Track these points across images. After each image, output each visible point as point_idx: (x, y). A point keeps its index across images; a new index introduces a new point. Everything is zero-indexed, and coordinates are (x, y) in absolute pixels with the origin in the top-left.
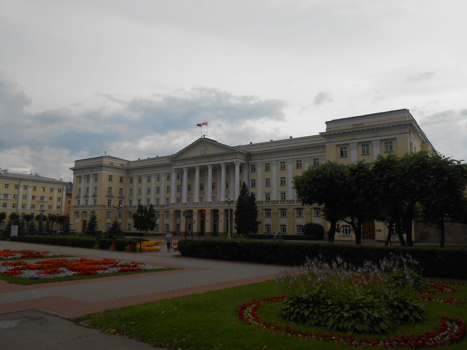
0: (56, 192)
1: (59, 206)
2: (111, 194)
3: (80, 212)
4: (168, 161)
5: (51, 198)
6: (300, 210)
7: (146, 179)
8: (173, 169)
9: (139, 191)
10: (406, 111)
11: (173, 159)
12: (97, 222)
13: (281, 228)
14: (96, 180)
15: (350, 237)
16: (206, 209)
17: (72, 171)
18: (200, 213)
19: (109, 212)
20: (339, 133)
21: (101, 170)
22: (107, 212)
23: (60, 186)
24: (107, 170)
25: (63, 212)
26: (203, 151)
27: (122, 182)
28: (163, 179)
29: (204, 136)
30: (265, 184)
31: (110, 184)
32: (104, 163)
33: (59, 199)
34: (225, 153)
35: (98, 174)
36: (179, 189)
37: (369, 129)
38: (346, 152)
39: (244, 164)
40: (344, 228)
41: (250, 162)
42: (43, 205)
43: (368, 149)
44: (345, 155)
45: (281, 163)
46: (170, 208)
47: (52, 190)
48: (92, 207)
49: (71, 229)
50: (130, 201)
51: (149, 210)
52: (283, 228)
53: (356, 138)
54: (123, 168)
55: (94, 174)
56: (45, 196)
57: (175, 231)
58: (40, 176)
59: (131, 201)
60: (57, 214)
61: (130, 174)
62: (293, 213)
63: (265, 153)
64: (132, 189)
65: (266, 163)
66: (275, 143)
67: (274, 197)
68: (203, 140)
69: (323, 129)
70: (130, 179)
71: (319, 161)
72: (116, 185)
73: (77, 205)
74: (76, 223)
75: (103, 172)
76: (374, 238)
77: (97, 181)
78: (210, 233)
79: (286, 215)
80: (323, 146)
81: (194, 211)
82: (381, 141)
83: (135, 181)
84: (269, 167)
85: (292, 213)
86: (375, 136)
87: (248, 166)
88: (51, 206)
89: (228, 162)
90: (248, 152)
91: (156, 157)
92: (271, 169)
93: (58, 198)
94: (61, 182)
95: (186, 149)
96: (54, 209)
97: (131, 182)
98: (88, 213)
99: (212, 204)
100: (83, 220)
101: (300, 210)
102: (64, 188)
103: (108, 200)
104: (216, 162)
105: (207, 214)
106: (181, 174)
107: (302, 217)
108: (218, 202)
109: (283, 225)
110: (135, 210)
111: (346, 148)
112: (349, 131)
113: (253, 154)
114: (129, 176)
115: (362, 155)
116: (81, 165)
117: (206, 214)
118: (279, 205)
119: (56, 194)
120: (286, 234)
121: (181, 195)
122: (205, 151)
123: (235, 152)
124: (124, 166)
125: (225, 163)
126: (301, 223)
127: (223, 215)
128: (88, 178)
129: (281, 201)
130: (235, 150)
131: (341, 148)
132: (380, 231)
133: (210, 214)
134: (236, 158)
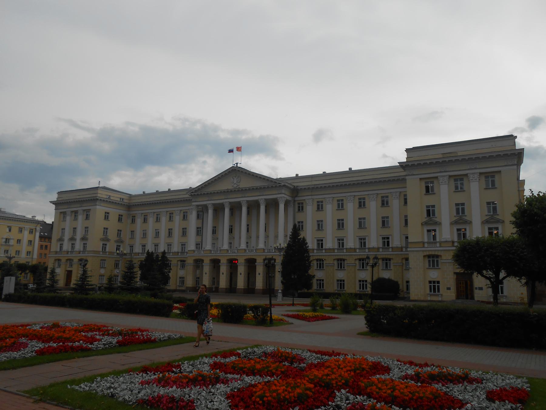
0: (26, 233)
1: (30, 252)
2: (108, 237)
3: (63, 260)
4: (187, 196)
5: (19, 241)
6: (341, 261)
9: (144, 233)
12: (135, 273)
13: (338, 284)
14: (87, 218)
15: (440, 296)
16: (204, 259)
17: (54, 206)
18: (229, 263)
19: (103, 260)
20: (430, 163)
21: (94, 205)
22: (101, 261)
23: (33, 226)
24: (102, 205)
25: (34, 259)
27: (121, 221)
28: (177, 218)
29: (237, 164)
30: (316, 228)
31: (106, 224)
32: (99, 195)
33: (30, 242)
34: (266, 187)
35: (90, 209)
36: (199, 231)
37: (465, 159)
38: (432, 187)
39: (290, 201)
40: (360, 283)
41: (297, 199)
42: (7, 249)
43: (462, 184)
44: (431, 192)
45: (338, 201)
46: (188, 256)
47: (21, 230)
48: (178, 255)
49: (90, 283)
50: (131, 246)
51: (161, 259)
52: (341, 284)
54: (123, 203)
55: (84, 210)
56: (11, 238)
57: (210, 287)
58: (5, 212)
59: (132, 247)
60: (26, 262)
61: (299, 197)
62: (354, 265)
63: (317, 187)
64: (134, 231)
65: (318, 201)
66: (329, 175)
67: (329, 243)
68: (236, 169)
69: (403, 158)
70: (131, 218)
71: (388, 200)
72: (113, 225)
73: (58, 250)
75: (98, 207)
76: (472, 298)
77: (89, 219)
78: (226, 288)
80: (402, 180)
81: (221, 261)
82: (449, 177)
83: (139, 221)
84: (322, 205)
86: (473, 168)
87: (294, 204)
88: (19, 251)
89: (221, 202)
90: (294, 186)
91: (168, 190)
92: (366, 206)
93: (29, 241)
94: (35, 221)
95: (216, 178)
96: (23, 255)
97: (133, 221)
98: (74, 261)
99: (247, 252)
100: (66, 271)
101: (341, 261)
102: (37, 228)
103: (103, 244)
104: (235, 199)
105: (205, 265)
106: (202, 213)
107: (366, 270)
108: (220, 251)
109: (433, 281)
111: (432, 182)
112: (445, 160)
113: (301, 189)
115: (455, 192)
116: (65, 197)
117: (239, 264)
119: (26, 236)
121: (202, 240)
122: (238, 184)
123: (279, 185)
124: (125, 201)
125: (265, 199)
128: (64, 216)
129: (338, 249)
130: (279, 183)
131: (426, 183)
132: (481, 289)
133: (227, 265)
134: (280, 194)
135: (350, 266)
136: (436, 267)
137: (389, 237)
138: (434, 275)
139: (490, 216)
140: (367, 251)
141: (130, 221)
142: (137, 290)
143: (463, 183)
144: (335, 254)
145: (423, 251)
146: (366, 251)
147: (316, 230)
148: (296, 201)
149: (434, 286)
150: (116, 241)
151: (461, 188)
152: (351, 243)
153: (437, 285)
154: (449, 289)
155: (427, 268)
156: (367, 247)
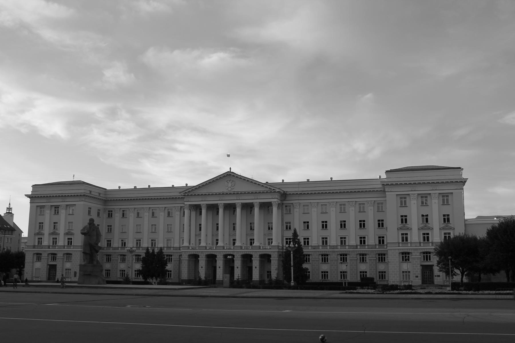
7: (134, 213)
8: (187, 205)
10: (461, 169)
11: (188, 193)
15: (70, 278)
16: (217, 254)
26: (230, 187)
41: (285, 202)
43: (426, 200)
46: (389, 249)
48: (64, 248)
53: (416, 190)
61: (286, 200)
62: (337, 259)
67: (334, 241)
70: (107, 212)
74: (36, 269)
76: (433, 282)
79: (327, 261)
85: (355, 259)
90: (284, 191)
97: (110, 215)
104: (212, 201)
110: (142, 253)
114: (106, 209)
117: (236, 259)
118: (140, 251)
120: (328, 281)
126: (384, 270)
127: (205, 261)
130: (274, 190)
132: (439, 276)
135: (255, 260)
136: (345, 262)
137: (346, 237)
138: (405, 266)
139: (424, 225)
140: (359, 248)
141: (106, 215)
142: (221, 284)
143: (427, 200)
144: (140, 251)
145: (398, 249)
146: (347, 248)
147: (303, 230)
148: (284, 204)
149: (382, 275)
150: (67, 234)
151: (426, 203)
152: (353, 240)
153: (170, 273)
154: (417, 277)
155: (401, 262)
156: (347, 245)
